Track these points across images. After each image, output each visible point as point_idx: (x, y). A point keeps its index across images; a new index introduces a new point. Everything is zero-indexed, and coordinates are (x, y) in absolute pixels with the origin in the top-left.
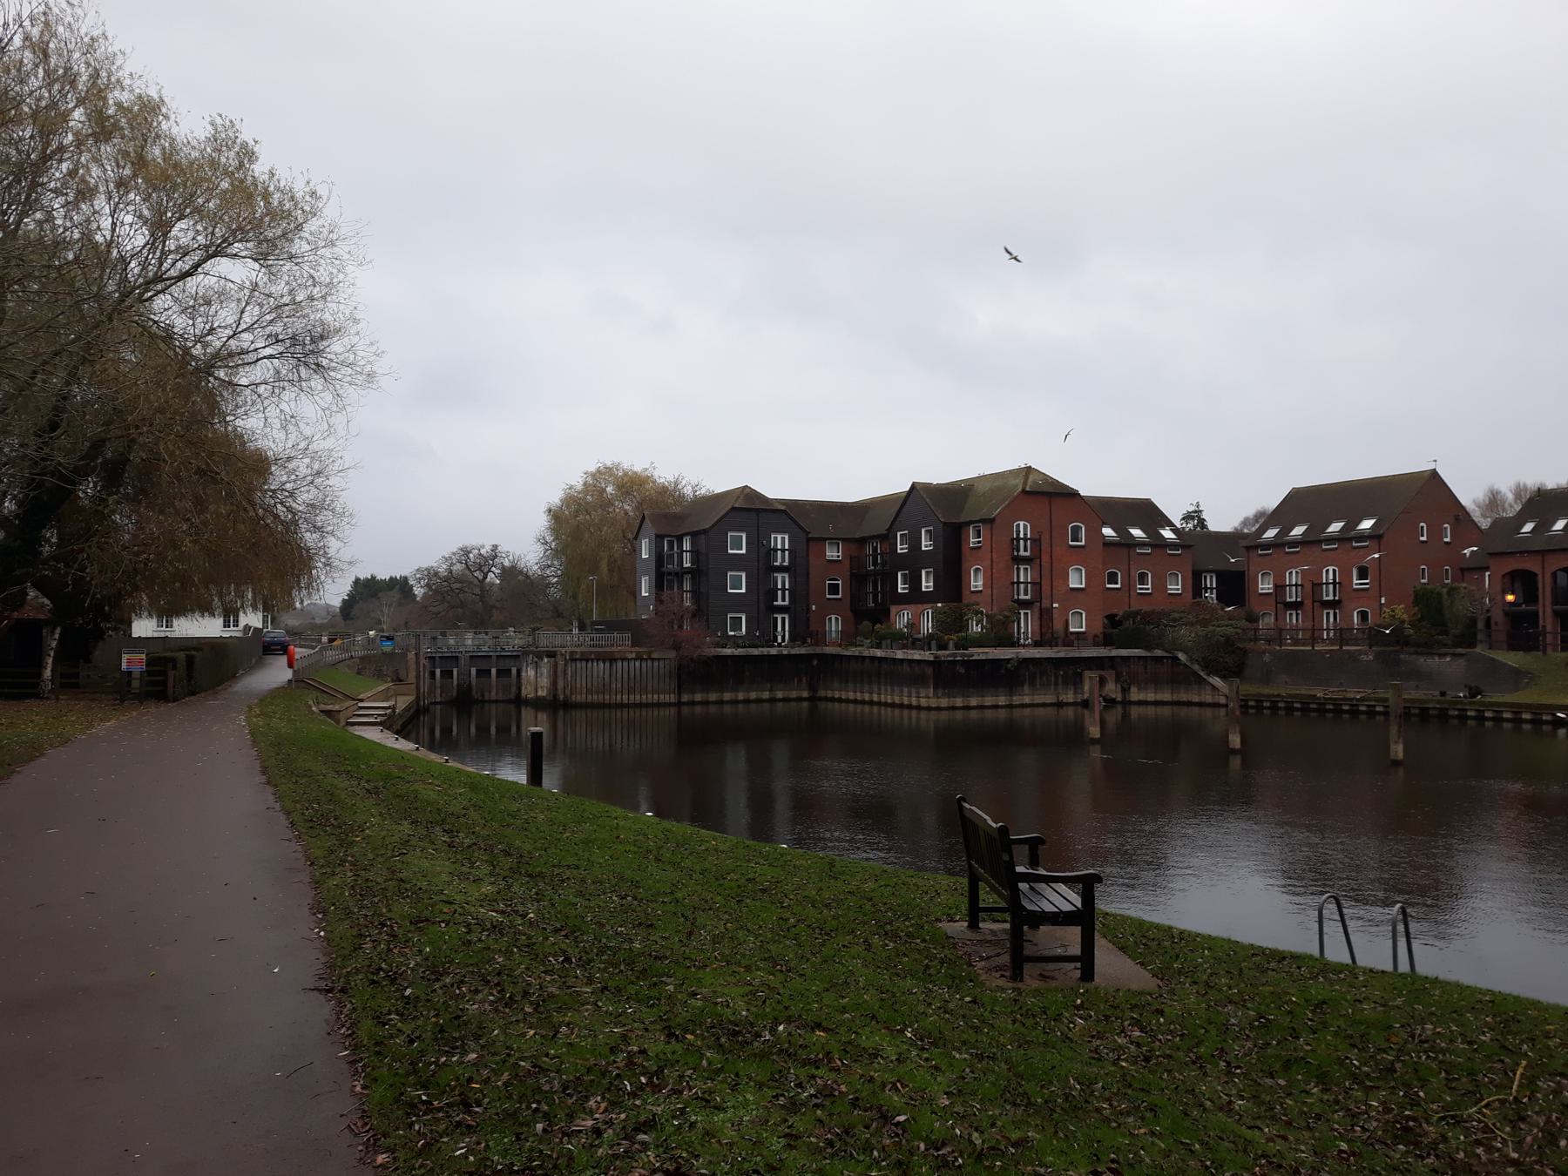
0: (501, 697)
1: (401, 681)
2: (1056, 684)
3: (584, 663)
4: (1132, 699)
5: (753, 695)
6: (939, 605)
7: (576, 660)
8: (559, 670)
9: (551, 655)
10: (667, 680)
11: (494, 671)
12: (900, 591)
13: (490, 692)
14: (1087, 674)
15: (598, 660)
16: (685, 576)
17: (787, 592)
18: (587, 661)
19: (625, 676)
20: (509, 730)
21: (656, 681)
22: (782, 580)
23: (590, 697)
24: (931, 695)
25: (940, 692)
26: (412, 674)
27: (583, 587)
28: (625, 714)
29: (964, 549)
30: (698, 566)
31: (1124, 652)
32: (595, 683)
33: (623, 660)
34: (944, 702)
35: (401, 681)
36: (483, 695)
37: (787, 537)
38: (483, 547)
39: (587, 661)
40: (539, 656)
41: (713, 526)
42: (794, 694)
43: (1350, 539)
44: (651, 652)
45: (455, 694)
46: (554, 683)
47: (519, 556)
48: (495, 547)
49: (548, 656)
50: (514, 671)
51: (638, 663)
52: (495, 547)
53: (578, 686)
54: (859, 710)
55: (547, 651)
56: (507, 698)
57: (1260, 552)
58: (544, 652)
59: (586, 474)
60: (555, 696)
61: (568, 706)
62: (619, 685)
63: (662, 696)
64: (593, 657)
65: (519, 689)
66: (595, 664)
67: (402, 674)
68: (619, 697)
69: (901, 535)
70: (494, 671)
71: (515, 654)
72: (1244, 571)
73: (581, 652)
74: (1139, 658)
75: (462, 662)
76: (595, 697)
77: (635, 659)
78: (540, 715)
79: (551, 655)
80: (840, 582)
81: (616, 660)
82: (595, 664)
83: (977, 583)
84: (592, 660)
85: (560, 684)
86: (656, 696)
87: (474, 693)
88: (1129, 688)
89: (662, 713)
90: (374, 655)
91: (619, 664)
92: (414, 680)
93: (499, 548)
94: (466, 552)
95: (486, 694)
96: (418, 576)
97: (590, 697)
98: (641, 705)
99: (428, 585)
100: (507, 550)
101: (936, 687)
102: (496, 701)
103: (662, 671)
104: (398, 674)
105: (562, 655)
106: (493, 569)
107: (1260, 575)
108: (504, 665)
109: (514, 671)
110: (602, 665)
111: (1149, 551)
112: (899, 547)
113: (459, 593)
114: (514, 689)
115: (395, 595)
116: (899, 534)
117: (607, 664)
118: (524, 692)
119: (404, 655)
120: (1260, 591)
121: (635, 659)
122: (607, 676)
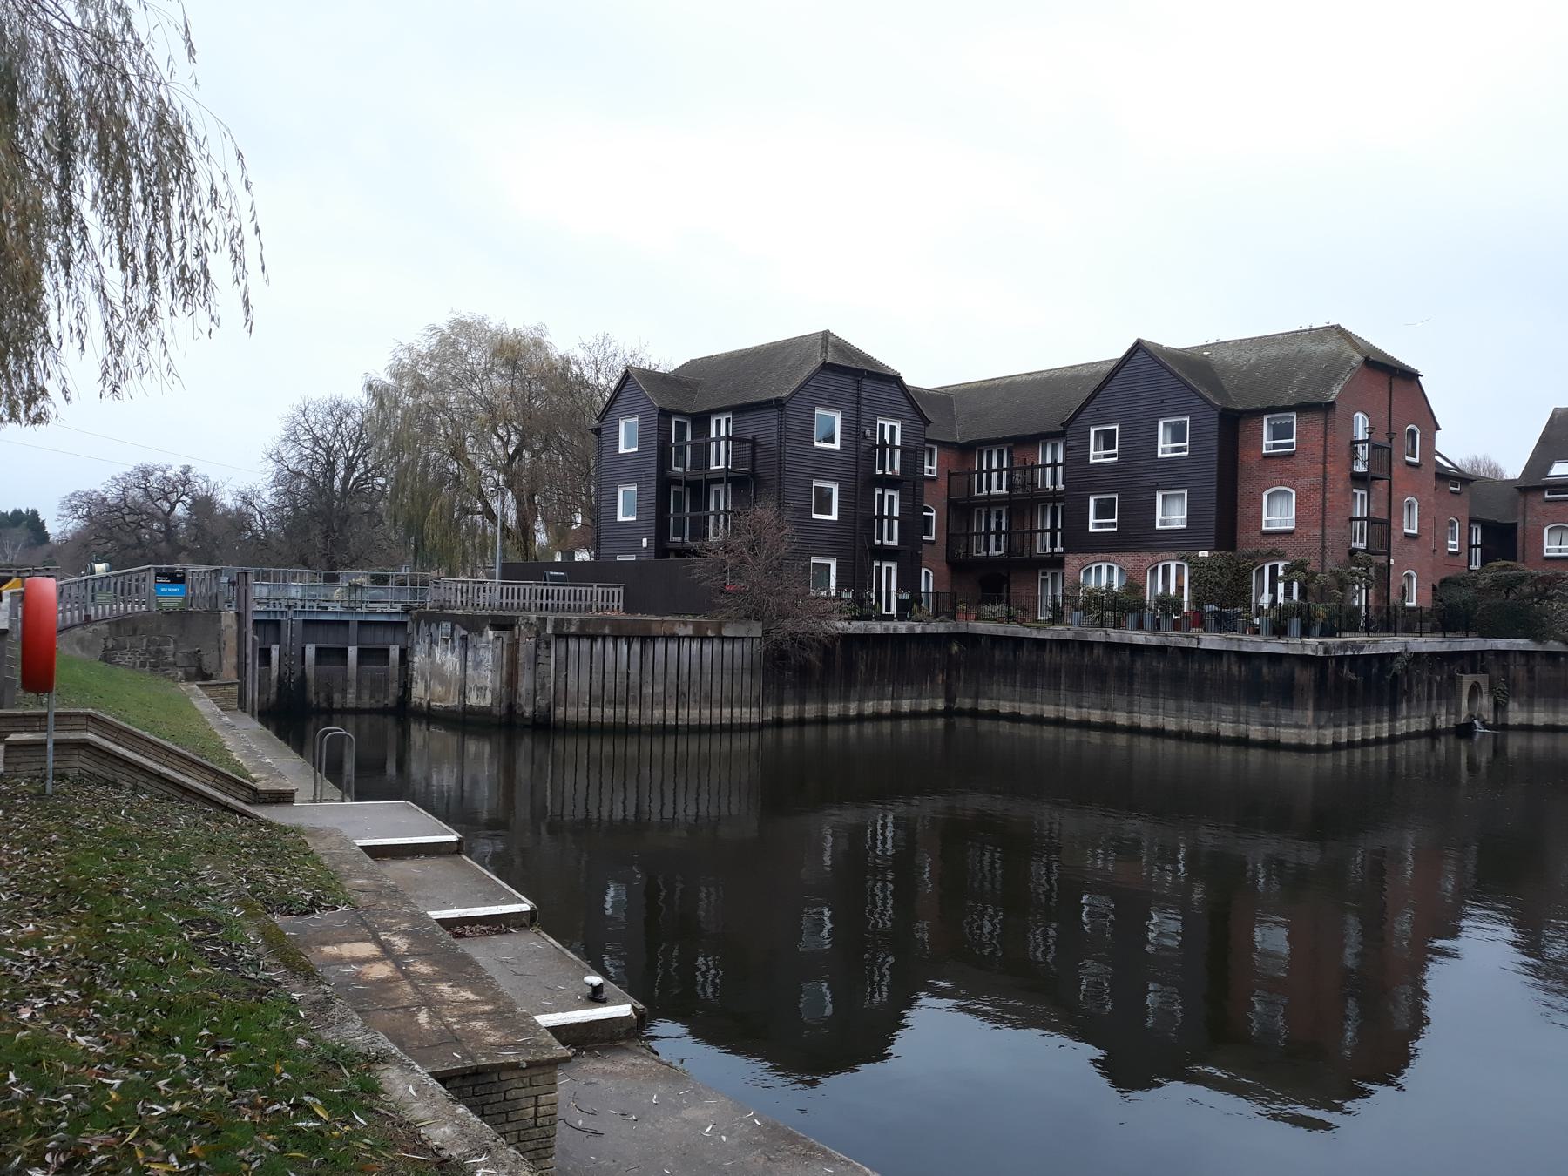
0: (367, 702)
1: (207, 677)
2: (1430, 699)
3: (585, 644)
4: (1510, 722)
5: (869, 707)
6: (1204, 554)
7: (567, 637)
8: (522, 655)
9: (503, 624)
10: (747, 679)
11: (352, 652)
12: (1091, 529)
13: (344, 692)
14: (1467, 681)
15: (616, 638)
16: (713, 488)
17: (896, 523)
18: (593, 638)
19: (672, 669)
20: (382, 768)
21: (727, 681)
22: (892, 502)
23: (596, 712)
24: (1309, 721)
25: (1324, 716)
26: (230, 661)
27: (435, 509)
28: (670, 748)
29: (1246, 456)
30: (753, 469)
31: (1501, 644)
32: (609, 684)
33: (667, 638)
34: (1328, 736)
35: (207, 677)
36: (329, 698)
37: (898, 427)
38: (170, 467)
39: (593, 638)
40: (474, 625)
41: (796, 392)
42: (925, 705)
43: (1541, 489)
44: (720, 625)
45: (273, 697)
46: (511, 681)
47: (216, 484)
48: (187, 470)
49: (494, 627)
50: (395, 652)
51: (695, 646)
52: (187, 470)
53: (572, 688)
54: (1344, 762)
55: (491, 616)
56: (381, 705)
57: (1547, 496)
58: (485, 617)
59: (432, 329)
60: (511, 707)
61: (544, 726)
62: (659, 689)
63: (737, 711)
64: (607, 631)
65: (406, 689)
66: (610, 646)
67: (209, 661)
68: (658, 713)
69: (1096, 432)
70: (352, 652)
71: (395, 619)
72: (1516, 524)
73: (581, 621)
74: (1522, 652)
75: (287, 632)
76: (609, 712)
77: (691, 638)
78: (472, 746)
79: (503, 624)
80: (933, 514)
81: (654, 639)
82: (610, 646)
83: (1279, 514)
84: (604, 637)
85: (525, 684)
86: (727, 712)
87: (311, 695)
88: (1506, 704)
89: (736, 744)
90: (145, 618)
91: (660, 646)
92: (233, 677)
93: (194, 471)
94: (146, 474)
95: (337, 697)
96: (74, 502)
97: (596, 712)
98: (700, 730)
99: (88, 515)
100: (203, 473)
101: (1318, 707)
102: (357, 712)
103: (738, 661)
104: (200, 660)
105: (529, 625)
106: (184, 498)
107: (1546, 530)
108: (376, 639)
109: (395, 652)
110: (625, 648)
111: (1458, 489)
112: (1092, 452)
113: (135, 528)
114: (394, 689)
115: (21, 534)
116: (1093, 431)
117: (636, 647)
118: (418, 692)
119: (214, 616)
120: (1546, 554)
121: (691, 638)
122: (635, 670)
